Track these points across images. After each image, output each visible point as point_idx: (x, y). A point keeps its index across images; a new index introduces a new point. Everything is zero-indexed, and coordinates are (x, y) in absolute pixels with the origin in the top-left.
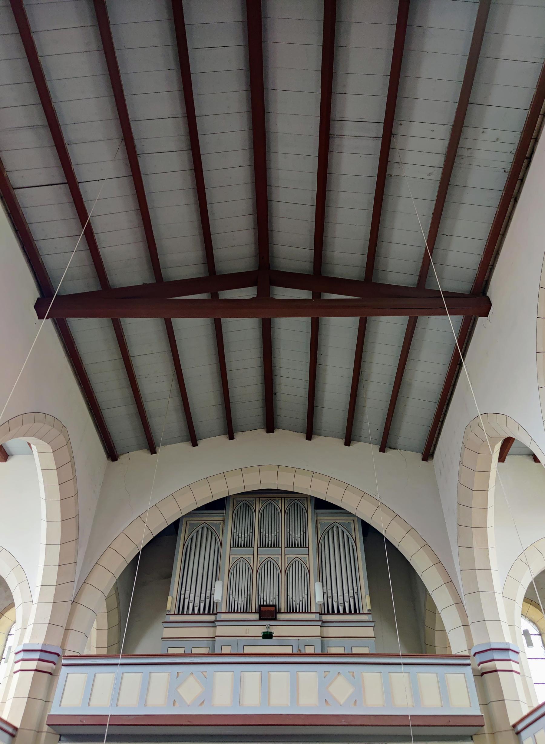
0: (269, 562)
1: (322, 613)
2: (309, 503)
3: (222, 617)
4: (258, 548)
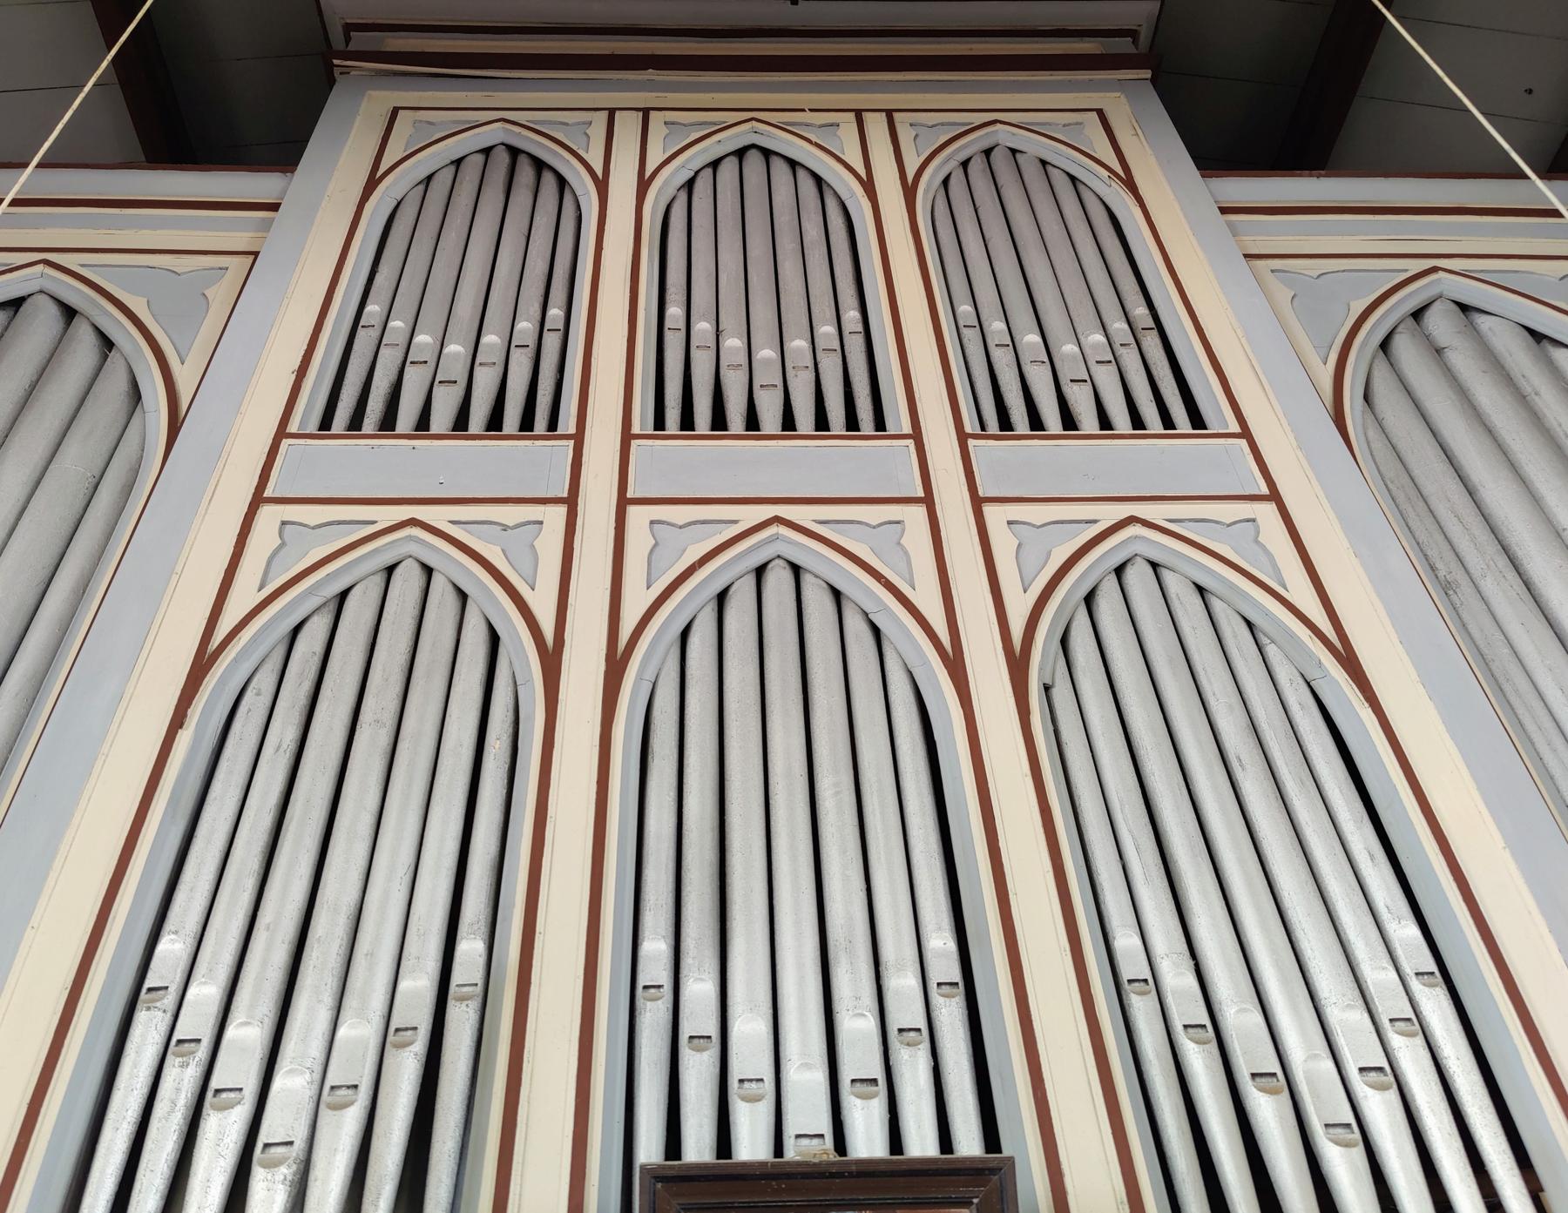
4: (634, 443)
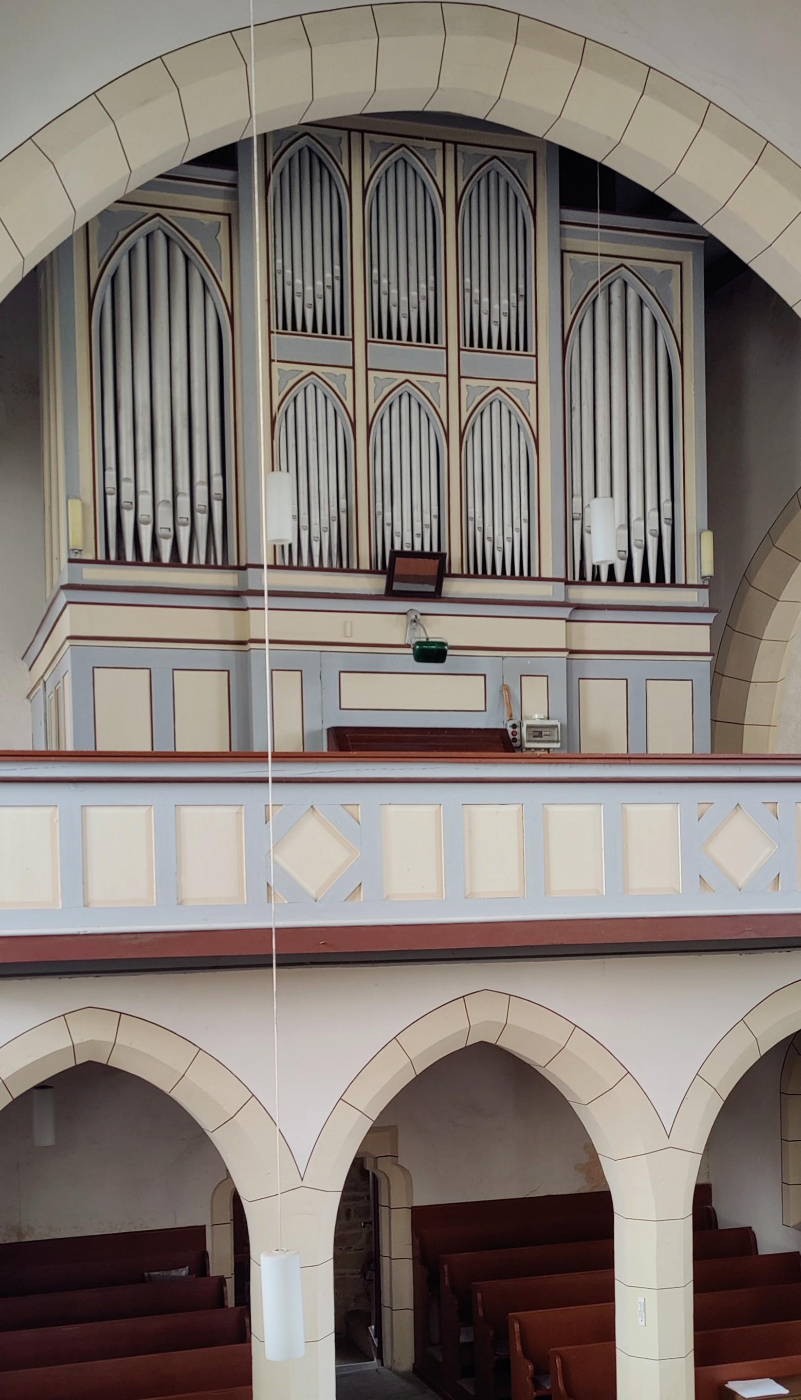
0: (405, 399)
1: (99, 558)
2: (541, 177)
3: (85, 576)
